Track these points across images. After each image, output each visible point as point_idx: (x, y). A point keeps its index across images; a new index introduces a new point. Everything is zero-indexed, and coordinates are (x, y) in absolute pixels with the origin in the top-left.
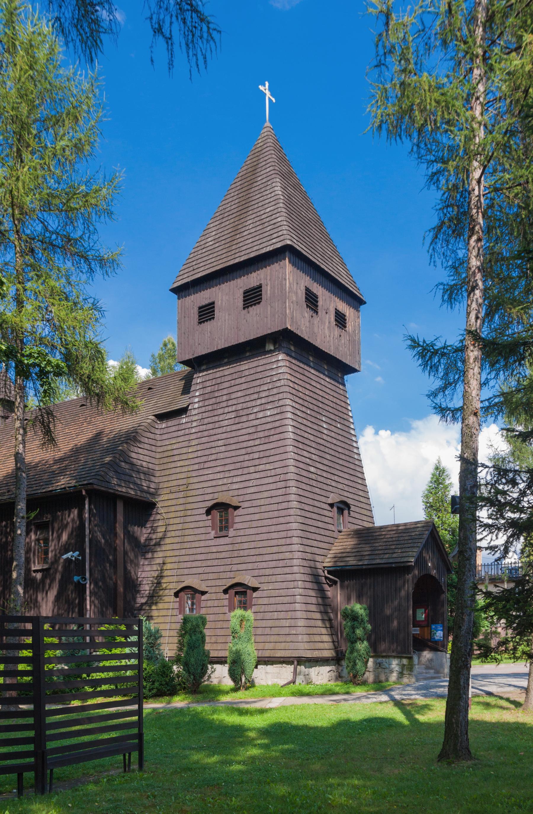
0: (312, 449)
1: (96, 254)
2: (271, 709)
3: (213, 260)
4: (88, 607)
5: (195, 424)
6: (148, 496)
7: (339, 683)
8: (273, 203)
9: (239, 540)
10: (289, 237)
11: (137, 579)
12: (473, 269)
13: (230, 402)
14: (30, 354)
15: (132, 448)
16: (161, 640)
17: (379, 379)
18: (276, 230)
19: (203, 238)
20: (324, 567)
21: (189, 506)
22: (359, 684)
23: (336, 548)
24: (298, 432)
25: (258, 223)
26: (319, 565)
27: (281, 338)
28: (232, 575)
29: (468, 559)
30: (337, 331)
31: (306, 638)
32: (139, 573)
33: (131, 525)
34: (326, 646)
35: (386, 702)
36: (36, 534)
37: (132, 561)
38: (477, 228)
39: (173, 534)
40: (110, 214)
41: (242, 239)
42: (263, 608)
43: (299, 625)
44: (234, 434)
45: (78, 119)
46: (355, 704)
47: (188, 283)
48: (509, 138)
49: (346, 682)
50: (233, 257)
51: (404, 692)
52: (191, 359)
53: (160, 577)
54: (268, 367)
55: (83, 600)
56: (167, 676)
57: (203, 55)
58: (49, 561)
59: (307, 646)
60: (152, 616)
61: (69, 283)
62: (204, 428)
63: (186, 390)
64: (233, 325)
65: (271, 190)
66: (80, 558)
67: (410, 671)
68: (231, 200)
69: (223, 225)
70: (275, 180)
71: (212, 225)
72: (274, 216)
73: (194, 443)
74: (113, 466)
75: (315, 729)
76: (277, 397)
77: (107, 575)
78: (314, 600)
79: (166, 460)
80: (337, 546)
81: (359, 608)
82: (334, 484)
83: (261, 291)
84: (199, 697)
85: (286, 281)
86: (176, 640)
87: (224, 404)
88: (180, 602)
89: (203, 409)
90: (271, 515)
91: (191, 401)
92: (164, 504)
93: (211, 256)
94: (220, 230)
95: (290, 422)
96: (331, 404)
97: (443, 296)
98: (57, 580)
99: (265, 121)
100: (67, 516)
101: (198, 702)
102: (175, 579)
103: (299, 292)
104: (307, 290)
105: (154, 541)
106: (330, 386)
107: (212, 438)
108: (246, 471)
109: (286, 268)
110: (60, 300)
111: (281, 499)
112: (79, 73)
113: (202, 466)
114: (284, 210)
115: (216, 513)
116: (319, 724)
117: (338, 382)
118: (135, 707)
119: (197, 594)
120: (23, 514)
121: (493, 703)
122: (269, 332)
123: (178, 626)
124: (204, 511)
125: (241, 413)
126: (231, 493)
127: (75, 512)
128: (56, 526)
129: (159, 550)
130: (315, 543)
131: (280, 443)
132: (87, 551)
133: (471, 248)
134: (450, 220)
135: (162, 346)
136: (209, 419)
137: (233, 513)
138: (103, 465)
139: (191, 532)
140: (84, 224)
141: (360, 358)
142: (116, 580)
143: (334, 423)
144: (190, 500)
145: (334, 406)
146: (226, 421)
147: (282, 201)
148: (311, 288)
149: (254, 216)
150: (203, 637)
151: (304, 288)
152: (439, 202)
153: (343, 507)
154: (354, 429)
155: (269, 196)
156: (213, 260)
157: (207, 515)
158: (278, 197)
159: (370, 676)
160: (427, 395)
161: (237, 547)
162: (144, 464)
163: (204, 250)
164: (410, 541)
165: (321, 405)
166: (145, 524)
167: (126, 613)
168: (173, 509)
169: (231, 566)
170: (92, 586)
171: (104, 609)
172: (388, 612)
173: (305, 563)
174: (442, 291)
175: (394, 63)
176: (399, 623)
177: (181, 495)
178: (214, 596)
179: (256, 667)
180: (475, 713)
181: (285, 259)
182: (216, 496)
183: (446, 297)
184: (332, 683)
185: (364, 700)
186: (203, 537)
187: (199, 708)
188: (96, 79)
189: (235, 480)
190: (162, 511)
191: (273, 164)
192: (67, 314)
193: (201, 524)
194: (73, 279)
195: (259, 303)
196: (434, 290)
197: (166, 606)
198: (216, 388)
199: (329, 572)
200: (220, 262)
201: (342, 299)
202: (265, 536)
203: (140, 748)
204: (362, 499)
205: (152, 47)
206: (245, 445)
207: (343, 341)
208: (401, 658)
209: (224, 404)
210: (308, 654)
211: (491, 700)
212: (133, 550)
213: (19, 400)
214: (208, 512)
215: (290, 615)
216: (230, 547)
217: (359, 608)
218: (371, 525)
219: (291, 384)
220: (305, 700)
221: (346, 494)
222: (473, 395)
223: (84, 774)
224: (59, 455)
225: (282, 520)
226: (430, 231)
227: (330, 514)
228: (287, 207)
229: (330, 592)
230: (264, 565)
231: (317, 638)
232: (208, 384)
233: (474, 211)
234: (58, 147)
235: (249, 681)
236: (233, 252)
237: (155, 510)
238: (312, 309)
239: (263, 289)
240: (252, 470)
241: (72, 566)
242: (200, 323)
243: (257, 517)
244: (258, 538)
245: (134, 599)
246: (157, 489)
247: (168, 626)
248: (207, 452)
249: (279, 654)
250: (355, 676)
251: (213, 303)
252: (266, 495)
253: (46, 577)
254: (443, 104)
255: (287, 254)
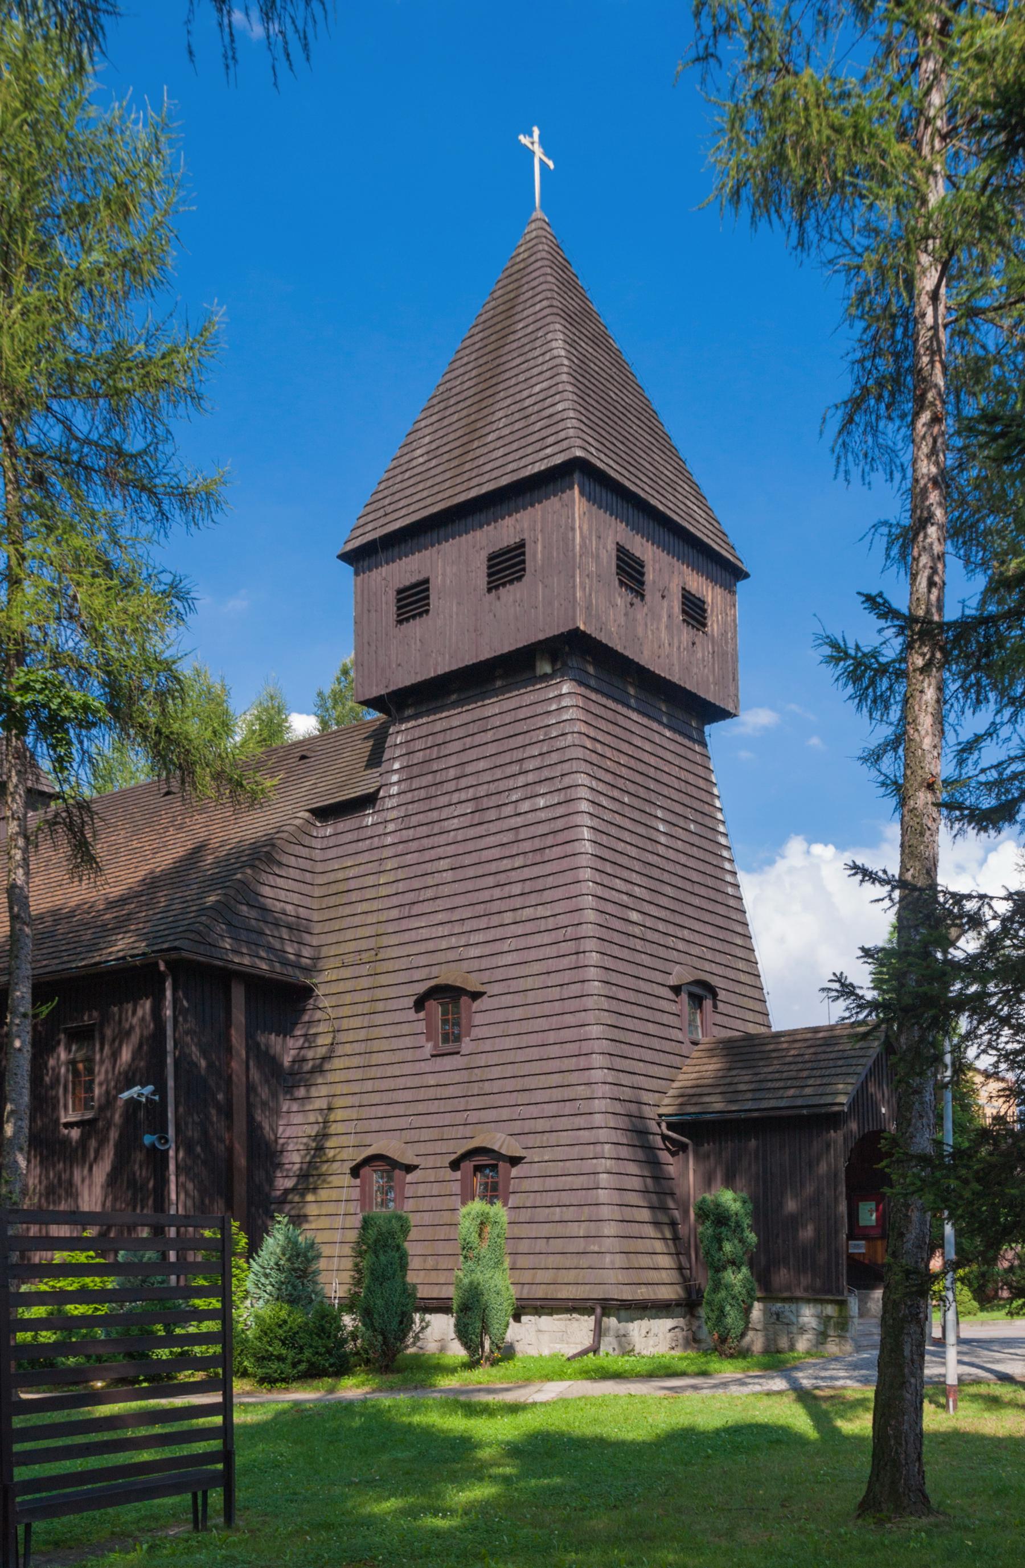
0: (634, 875)
1: (173, 484)
2: (534, 1404)
3: (425, 494)
4: (173, 1196)
5: (391, 827)
6: (298, 972)
7: (691, 1353)
8: (548, 374)
9: (482, 1059)
10: (579, 442)
11: (276, 1141)
12: (922, 482)
13: (464, 782)
14: (27, 684)
15: (264, 877)
16: (322, 1264)
17: (815, 741)
18: (553, 429)
19: (406, 450)
20: (660, 1116)
21: (380, 993)
22: (731, 1356)
23: (685, 1076)
24: (604, 840)
25: (517, 416)
26: (648, 1112)
27: (567, 648)
28: (468, 1131)
29: (916, 1092)
30: (686, 634)
31: (619, 1260)
32: (281, 1129)
33: (263, 1032)
34: (665, 1276)
35: (780, 1393)
36: (69, 1050)
37: (264, 1104)
38: (930, 396)
39: (348, 1049)
40: (197, 398)
41: (485, 450)
42: (530, 1200)
43: (606, 1233)
44: (470, 846)
45: (128, 209)
46: (714, 1397)
47: (374, 541)
48: (990, 197)
49: (706, 1353)
50: (466, 486)
51: (823, 1374)
52: (382, 696)
53: (323, 1136)
54: (539, 709)
55: (162, 1183)
56: (329, 1337)
57: (297, 31)
58: (95, 1104)
59: (622, 1276)
60: (306, 1216)
61: (116, 543)
62: (410, 834)
63: (375, 759)
64: (468, 624)
65: (544, 349)
66: (157, 1098)
67: (842, 1329)
68: (461, 370)
69: (446, 422)
70: (551, 327)
71: (423, 424)
72: (549, 401)
73: (389, 865)
74: (223, 911)
75: (620, 1446)
76: (557, 771)
77: (211, 1133)
78: (636, 1183)
79: (332, 901)
80: (687, 1072)
81: (729, 1199)
82: (681, 945)
83: (523, 554)
84: (395, 1378)
85: (575, 530)
86: (348, 1264)
87: (451, 786)
88: (362, 1187)
89: (409, 797)
90: (547, 1009)
91: (383, 780)
92: (330, 988)
93: (421, 486)
94: (441, 433)
95: (587, 820)
96: (676, 784)
97: (888, 549)
98: (112, 1143)
99: (534, 208)
100: (130, 1013)
101: (391, 1389)
102: (352, 1140)
103: (604, 555)
104: (621, 549)
105: (311, 1063)
106: (672, 746)
107: (428, 855)
108: (495, 920)
109: (576, 509)
110: (94, 575)
111: (567, 977)
112: (133, 116)
113: (406, 911)
114: (570, 388)
115: (435, 1007)
116: (630, 1436)
117: (690, 738)
118: (215, 1398)
119: (397, 1171)
120: (25, 1007)
121: (1007, 1398)
122: (541, 637)
123: (353, 1236)
124: (410, 1002)
125: (486, 803)
126: (465, 966)
127: (146, 1006)
128: (109, 1032)
129: (320, 1081)
130: (640, 1067)
131: (565, 864)
132: (171, 1083)
133: (918, 440)
134: (880, 384)
135: (338, 673)
136: (421, 816)
137: (470, 1007)
138: (203, 910)
139: (384, 1045)
140: (144, 421)
141: (737, 688)
142: (231, 1140)
143: (681, 822)
144: (383, 980)
145: (683, 786)
146: (456, 821)
147: (565, 369)
148: (627, 547)
149: (509, 401)
150: (403, 1257)
151: (614, 546)
152: (857, 345)
153: (701, 993)
154: (726, 835)
155: (540, 360)
156: (425, 494)
157: (417, 1011)
158: (557, 361)
159: (755, 1340)
160: (860, 758)
161: (478, 1074)
162: (289, 908)
163: (407, 475)
164: (840, 1063)
165: (652, 785)
166: (292, 1030)
167: (253, 1209)
168: (348, 998)
169: (466, 1114)
170: (181, 1154)
171: (207, 1201)
172: (791, 1205)
173: (618, 1108)
174: (885, 539)
175: (735, 49)
176: (818, 1231)
177: (365, 969)
178: (431, 1175)
179: (517, 1318)
180: (934, 1419)
181: (572, 488)
182: (435, 971)
183: (895, 552)
184: (678, 1353)
185: (734, 1389)
186: (409, 1055)
187: (386, 1400)
188: (165, 127)
189: (474, 938)
190: (324, 1003)
191: (549, 294)
192: (108, 603)
193: (405, 1029)
194: (124, 533)
195: (519, 579)
196: (869, 537)
197: (334, 1194)
198: (435, 753)
199: (670, 1126)
200: (440, 496)
201: (696, 568)
202: (535, 1053)
203: (227, 1481)
204: (743, 978)
205: (188, 22)
206: (493, 867)
207: (700, 655)
208: (822, 1302)
209: (451, 786)
210: (627, 1294)
211: (1005, 1391)
212: (267, 1081)
213: (15, 780)
214: (420, 1004)
215: (586, 1213)
216: (463, 1076)
217: (729, 1199)
218: (763, 1030)
219: (589, 744)
220: (608, 1387)
221: (707, 966)
222: (925, 747)
223: (113, 1533)
224: (116, 891)
225: (570, 1020)
226: (836, 407)
227: (673, 1008)
228: (576, 383)
229: (672, 1164)
230: (534, 1111)
231: (645, 1261)
232: (419, 745)
233: (925, 359)
234: (83, 267)
235: (499, 1348)
236: (466, 476)
237: (311, 1001)
238: (632, 589)
239: (527, 549)
240: (508, 918)
241: (142, 1114)
242: (400, 622)
243: (518, 1013)
244: (521, 1055)
245: (271, 1181)
246: (316, 959)
247: (337, 1236)
248: (417, 884)
249: (565, 1293)
250: (723, 1340)
251: (426, 581)
252: (536, 968)
253: (89, 1137)
254: (849, 132)
255: (577, 476)
